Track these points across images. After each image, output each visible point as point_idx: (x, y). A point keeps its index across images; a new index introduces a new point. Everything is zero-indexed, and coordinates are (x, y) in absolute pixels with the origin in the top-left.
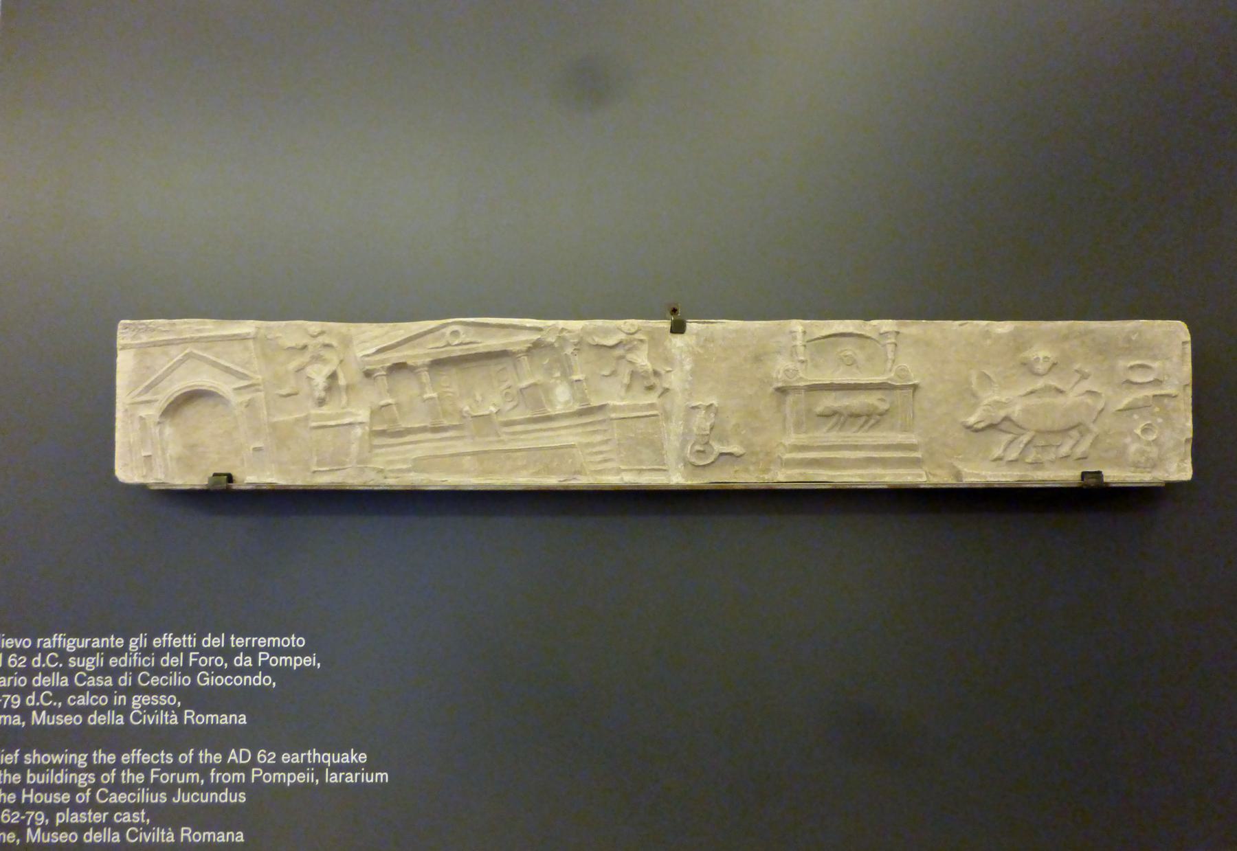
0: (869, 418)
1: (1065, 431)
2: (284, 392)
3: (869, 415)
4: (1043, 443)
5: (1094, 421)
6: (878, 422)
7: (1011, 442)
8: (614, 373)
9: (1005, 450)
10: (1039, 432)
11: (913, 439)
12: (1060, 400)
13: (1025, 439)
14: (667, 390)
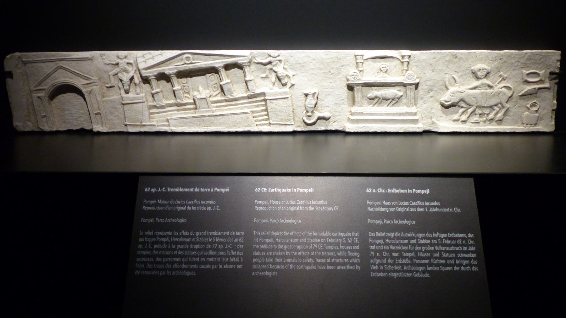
0: (395, 101)
1: (491, 107)
2: (108, 86)
3: (393, 99)
4: (480, 112)
5: (507, 102)
6: (397, 102)
7: (464, 112)
8: (267, 77)
9: (460, 116)
10: (479, 107)
11: (413, 109)
12: (491, 90)
13: (470, 111)
14: (293, 85)
